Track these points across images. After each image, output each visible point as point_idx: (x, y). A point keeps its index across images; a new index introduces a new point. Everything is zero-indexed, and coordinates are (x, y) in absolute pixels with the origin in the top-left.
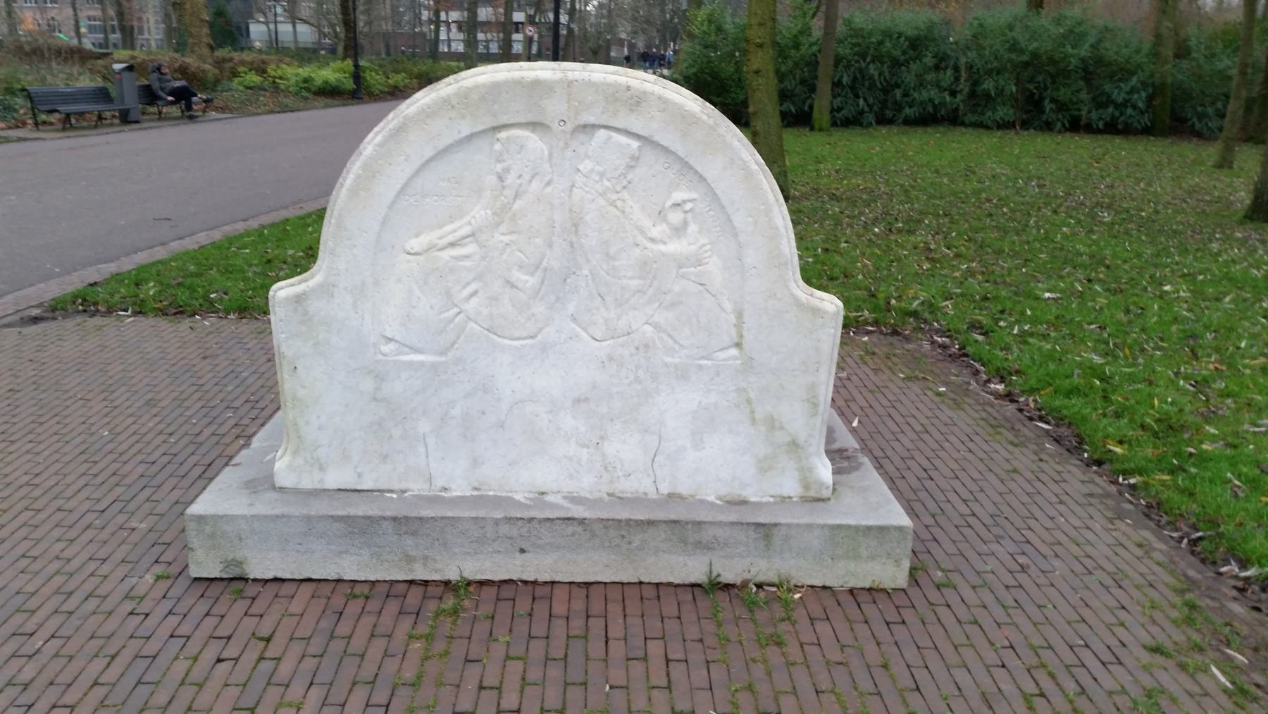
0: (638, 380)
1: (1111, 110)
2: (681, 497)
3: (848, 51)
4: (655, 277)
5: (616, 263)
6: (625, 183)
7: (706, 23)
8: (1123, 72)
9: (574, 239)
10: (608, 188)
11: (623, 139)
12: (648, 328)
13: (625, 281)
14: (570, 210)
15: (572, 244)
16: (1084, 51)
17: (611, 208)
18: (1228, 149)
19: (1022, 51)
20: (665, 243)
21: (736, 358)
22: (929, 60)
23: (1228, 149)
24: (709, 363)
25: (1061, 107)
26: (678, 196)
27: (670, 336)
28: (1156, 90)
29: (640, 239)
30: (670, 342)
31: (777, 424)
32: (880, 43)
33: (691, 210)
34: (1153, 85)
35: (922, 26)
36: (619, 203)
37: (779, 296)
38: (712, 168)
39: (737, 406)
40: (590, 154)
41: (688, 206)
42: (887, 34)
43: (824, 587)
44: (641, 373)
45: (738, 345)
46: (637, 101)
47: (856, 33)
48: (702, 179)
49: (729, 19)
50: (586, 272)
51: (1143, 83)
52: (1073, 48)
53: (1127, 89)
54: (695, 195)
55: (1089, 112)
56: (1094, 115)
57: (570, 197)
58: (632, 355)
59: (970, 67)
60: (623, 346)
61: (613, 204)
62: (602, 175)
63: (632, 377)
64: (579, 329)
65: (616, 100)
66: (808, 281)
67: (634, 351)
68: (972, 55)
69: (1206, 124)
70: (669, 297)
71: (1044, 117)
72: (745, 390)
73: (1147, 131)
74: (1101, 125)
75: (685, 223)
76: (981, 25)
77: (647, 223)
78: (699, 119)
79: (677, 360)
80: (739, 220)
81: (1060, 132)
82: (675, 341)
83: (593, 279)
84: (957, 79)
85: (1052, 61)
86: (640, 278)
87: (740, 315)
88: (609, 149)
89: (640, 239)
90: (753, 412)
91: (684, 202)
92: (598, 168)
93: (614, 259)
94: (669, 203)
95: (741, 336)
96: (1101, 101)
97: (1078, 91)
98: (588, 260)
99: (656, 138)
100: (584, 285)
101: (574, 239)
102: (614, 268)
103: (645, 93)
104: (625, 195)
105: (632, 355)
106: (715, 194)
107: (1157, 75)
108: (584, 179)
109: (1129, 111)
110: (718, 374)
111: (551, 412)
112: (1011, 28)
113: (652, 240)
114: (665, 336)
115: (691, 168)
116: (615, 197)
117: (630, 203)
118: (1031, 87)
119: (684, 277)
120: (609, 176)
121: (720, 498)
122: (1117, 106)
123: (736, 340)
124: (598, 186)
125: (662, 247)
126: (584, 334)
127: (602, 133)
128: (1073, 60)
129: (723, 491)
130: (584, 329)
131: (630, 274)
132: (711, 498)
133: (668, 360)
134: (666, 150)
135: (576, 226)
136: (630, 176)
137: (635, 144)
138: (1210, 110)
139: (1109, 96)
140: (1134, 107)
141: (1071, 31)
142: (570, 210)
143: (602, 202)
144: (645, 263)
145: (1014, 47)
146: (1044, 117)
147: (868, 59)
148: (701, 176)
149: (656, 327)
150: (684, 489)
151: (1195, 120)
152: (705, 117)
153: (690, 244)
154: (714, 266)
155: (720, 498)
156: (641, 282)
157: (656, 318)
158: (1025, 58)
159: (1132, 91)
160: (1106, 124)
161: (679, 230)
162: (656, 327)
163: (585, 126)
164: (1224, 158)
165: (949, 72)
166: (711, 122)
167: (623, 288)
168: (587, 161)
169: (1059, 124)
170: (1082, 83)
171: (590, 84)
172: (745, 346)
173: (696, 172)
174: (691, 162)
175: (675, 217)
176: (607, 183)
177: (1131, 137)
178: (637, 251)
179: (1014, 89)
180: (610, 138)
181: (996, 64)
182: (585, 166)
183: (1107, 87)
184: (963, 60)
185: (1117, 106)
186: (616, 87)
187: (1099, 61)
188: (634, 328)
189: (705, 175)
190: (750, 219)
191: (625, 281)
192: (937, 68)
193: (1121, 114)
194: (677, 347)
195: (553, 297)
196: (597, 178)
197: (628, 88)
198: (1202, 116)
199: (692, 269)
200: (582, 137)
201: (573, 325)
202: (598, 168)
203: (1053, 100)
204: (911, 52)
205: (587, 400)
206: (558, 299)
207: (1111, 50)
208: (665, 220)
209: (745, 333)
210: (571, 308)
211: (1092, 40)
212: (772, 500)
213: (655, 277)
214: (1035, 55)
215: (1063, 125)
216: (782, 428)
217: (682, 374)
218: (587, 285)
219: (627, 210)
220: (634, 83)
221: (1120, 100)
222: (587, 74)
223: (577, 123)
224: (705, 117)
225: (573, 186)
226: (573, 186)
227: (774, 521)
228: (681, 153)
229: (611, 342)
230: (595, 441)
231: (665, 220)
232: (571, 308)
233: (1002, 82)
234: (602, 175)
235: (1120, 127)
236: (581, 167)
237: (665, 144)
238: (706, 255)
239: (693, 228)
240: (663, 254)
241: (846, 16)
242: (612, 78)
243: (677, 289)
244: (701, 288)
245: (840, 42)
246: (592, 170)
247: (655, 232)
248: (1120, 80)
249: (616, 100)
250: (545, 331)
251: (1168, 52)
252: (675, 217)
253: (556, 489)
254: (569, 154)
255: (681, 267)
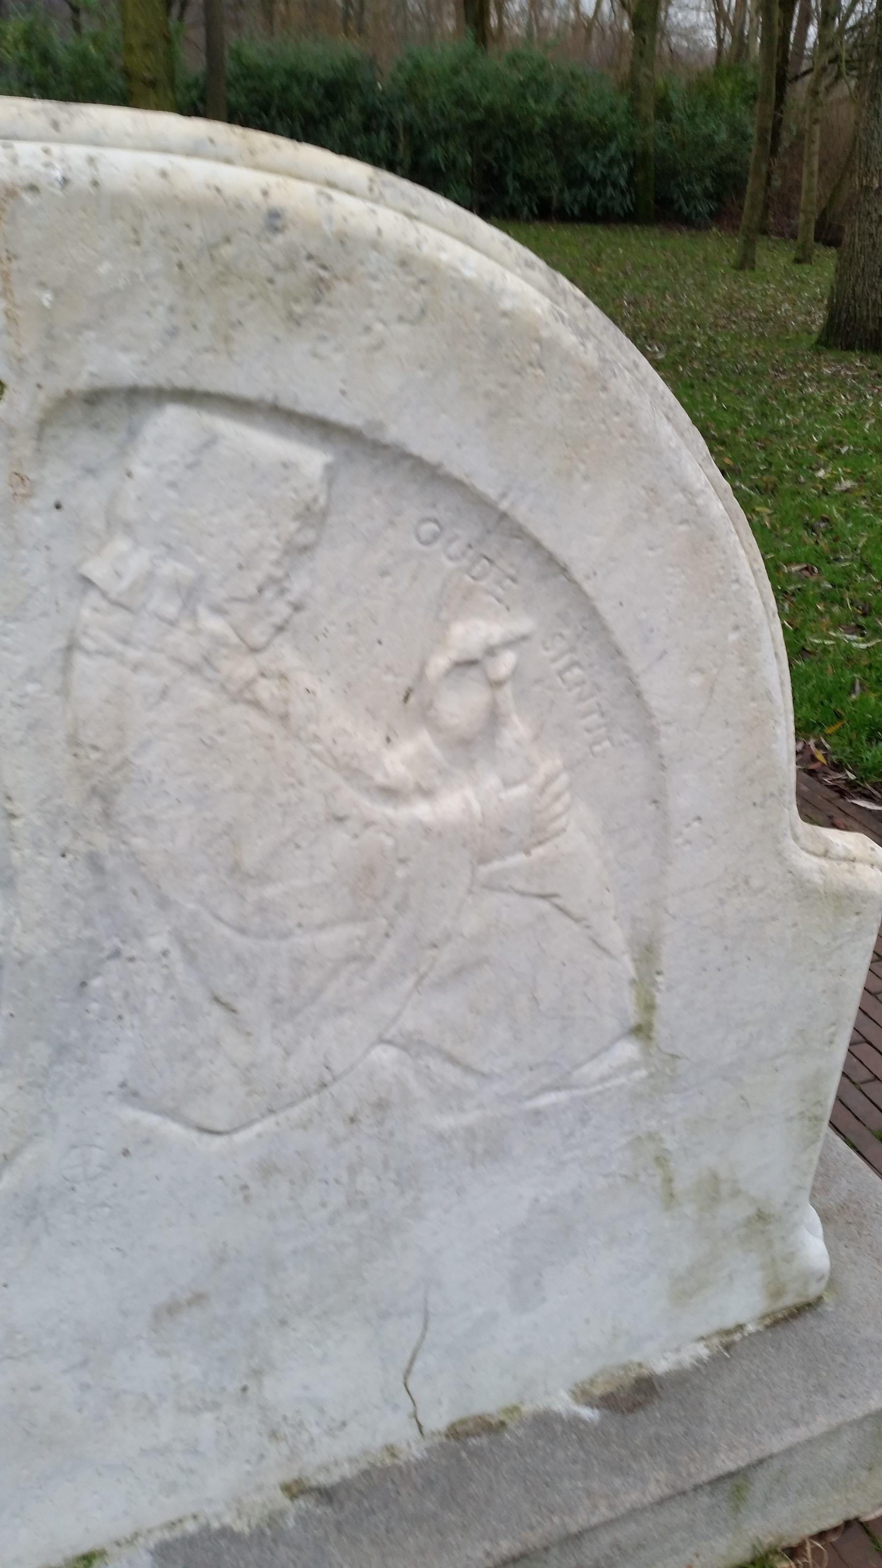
0: (357, 1201)
1: (587, 189)
2: (489, 1427)
3: (243, 100)
4: (401, 907)
5: (271, 892)
6: (282, 610)
7: (22, 47)
8: (595, 136)
9: (102, 841)
10: (219, 641)
11: (265, 443)
12: (385, 1055)
13: (302, 941)
14: (74, 741)
15: (95, 863)
16: (550, 108)
17: (239, 711)
18: (750, 244)
19: (473, 107)
20: (427, 793)
21: (633, 1066)
22: (355, 116)
23: (750, 244)
24: (562, 1097)
25: (527, 185)
26: (471, 633)
27: (453, 1060)
28: (638, 160)
29: (350, 798)
30: (453, 1075)
31: (725, 1189)
32: (285, 89)
33: (516, 673)
34: (634, 154)
35: (339, 65)
36: (266, 690)
37: (756, 883)
38: (587, 529)
39: (630, 1179)
40: (130, 511)
41: (506, 662)
42: (293, 74)
43: (848, 1524)
44: (366, 1181)
45: (641, 1031)
46: (314, 277)
47: (249, 72)
48: (553, 566)
49: (57, 40)
50: (157, 943)
51: (625, 155)
52: (537, 101)
53: (606, 160)
54: (524, 624)
55: (561, 191)
56: (567, 196)
57: (64, 691)
58: (336, 1141)
59: (409, 128)
60: (305, 1125)
61: (243, 695)
62: (189, 594)
63: (337, 1199)
64: (152, 1120)
65: (225, 275)
66: (807, 817)
67: (341, 1129)
68: (411, 110)
69: (695, 207)
70: (446, 956)
71: (507, 201)
72: (652, 1136)
73: (631, 218)
74: (576, 211)
75: (494, 719)
76: (418, 66)
77: (366, 739)
78: (548, 346)
79: (471, 1117)
80: (662, 688)
81: (527, 221)
82: (468, 1069)
83: (191, 958)
84: (394, 146)
85: (511, 120)
86: (353, 917)
87: (647, 953)
88: (199, 488)
89: (350, 798)
90: (669, 1180)
91: (491, 651)
92: (168, 568)
93: (262, 878)
94: (440, 663)
95: (649, 1007)
96: (574, 178)
97: (547, 162)
98: (164, 903)
99: (393, 433)
100: (156, 983)
101: (102, 841)
102: (262, 908)
103: (343, 240)
104: (285, 654)
105: (336, 1141)
106: (594, 613)
107: (638, 142)
108: (118, 618)
109: (610, 190)
110: (584, 1120)
111: (84, 1363)
112: (456, 71)
113: (390, 793)
114: (435, 1064)
115: (519, 532)
116: (246, 668)
117: (306, 680)
118: (489, 157)
119: (491, 886)
120: (220, 594)
121: (582, 1395)
122: (593, 183)
123: (634, 1019)
124: (180, 640)
125: (422, 810)
126: (174, 1129)
127: (173, 423)
128: (539, 120)
129: (584, 1370)
130: (173, 1114)
131: (318, 915)
132: (562, 1402)
133: (446, 1122)
134: (430, 475)
135: (103, 795)
136: (298, 586)
137: (312, 460)
138: (698, 189)
139: (584, 171)
140: (615, 185)
141: (532, 79)
142: (74, 741)
143: (201, 694)
144: (370, 871)
145: (462, 100)
146: (507, 201)
147: (273, 112)
148: (551, 559)
149: (410, 1044)
150: (488, 1402)
151: (682, 201)
152: (570, 339)
153: (508, 784)
154: (578, 834)
155: (582, 1395)
156: (359, 930)
157: (408, 1023)
158: (478, 116)
159: (612, 162)
160: (582, 210)
161: (471, 746)
162: (410, 1044)
163: (95, 398)
164: (745, 256)
165: (383, 134)
166: (590, 357)
167: (299, 962)
168: (121, 545)
169: (525, 211)
170: (549, 153)
171: (99, 203)
172: (661, 1032)
173: (537, 545)
174: (521, 513)
175: (461, 705)
176: (214, 624)
177: (613, 226)
178: (341, 838)
179: (469, 159)
180: (211, 441)
181: (443, 124)
182: (118, 562)
183: (581, 158)
184: (399, 118)
185: (593, 183)
186: (219, 212)
187: (567, 120)
188: (338, 1067)
189: (564, 554)
190: (696, 680)
191: (302, 941)
192: (367, 129)
193: (599, 194)
194: (471, 1082)
195: (41, 1052)
196: (171, 609)
197: (275, 221)
198: (689, 197)
199: (520, 858)
200: (87, 445)
201: (130, 1113)
202: (168, 568)
203: (517, 176)
204: (328, 104)
205: (199, 1299)
206: (62, 1050)
207: (581, 106)
208: (426, 715)
209: (659, 999)
210: (115, 1066)
211: (557, 90)
212: (703, 1351)
213: (401, 907)
214: (490, 111)
215: (531, 210)
216: (736, 1193)
217: (486, 1148)
218: (169, 980)
219: (298, 708)
220: (296, 196)
221: (598, 176)
222: (77, 153)
223: (58, 384)
224: (570, 339)
225: (71, 647)
226: (71, 647)
227: (757, 1453)
228: (487, 484)
229: (267, 1125)
230: (233, 1386)
231: (426, 715)
232: (115, 1066)
233: (452, 149)
234: (189, 594)
235: (599, 212)
236: (97, 569)
237: (431, 452)
238: (558, 807)
239: (517, 730)
240: (427, 830)
241: (233, 45)
242: (197, 174)
243: (471, 924)
244: (544, 906)
245: (229, 85)
246: (148, 578)
247: (396, 763)
248: (596, 148)
249: (225, 275)
250: (28, 1156)
251: (648, 110)
252: (461, 705)
253: (125, 1529)
254: (37, 521)
255: (484, 860)
